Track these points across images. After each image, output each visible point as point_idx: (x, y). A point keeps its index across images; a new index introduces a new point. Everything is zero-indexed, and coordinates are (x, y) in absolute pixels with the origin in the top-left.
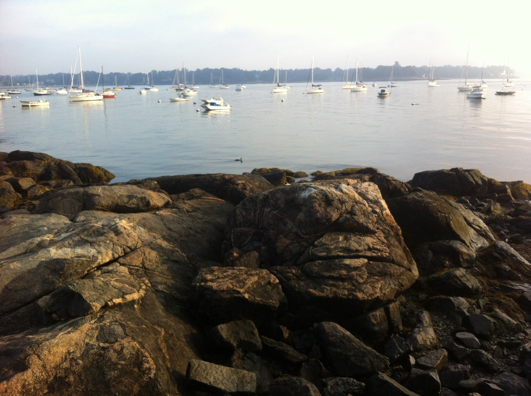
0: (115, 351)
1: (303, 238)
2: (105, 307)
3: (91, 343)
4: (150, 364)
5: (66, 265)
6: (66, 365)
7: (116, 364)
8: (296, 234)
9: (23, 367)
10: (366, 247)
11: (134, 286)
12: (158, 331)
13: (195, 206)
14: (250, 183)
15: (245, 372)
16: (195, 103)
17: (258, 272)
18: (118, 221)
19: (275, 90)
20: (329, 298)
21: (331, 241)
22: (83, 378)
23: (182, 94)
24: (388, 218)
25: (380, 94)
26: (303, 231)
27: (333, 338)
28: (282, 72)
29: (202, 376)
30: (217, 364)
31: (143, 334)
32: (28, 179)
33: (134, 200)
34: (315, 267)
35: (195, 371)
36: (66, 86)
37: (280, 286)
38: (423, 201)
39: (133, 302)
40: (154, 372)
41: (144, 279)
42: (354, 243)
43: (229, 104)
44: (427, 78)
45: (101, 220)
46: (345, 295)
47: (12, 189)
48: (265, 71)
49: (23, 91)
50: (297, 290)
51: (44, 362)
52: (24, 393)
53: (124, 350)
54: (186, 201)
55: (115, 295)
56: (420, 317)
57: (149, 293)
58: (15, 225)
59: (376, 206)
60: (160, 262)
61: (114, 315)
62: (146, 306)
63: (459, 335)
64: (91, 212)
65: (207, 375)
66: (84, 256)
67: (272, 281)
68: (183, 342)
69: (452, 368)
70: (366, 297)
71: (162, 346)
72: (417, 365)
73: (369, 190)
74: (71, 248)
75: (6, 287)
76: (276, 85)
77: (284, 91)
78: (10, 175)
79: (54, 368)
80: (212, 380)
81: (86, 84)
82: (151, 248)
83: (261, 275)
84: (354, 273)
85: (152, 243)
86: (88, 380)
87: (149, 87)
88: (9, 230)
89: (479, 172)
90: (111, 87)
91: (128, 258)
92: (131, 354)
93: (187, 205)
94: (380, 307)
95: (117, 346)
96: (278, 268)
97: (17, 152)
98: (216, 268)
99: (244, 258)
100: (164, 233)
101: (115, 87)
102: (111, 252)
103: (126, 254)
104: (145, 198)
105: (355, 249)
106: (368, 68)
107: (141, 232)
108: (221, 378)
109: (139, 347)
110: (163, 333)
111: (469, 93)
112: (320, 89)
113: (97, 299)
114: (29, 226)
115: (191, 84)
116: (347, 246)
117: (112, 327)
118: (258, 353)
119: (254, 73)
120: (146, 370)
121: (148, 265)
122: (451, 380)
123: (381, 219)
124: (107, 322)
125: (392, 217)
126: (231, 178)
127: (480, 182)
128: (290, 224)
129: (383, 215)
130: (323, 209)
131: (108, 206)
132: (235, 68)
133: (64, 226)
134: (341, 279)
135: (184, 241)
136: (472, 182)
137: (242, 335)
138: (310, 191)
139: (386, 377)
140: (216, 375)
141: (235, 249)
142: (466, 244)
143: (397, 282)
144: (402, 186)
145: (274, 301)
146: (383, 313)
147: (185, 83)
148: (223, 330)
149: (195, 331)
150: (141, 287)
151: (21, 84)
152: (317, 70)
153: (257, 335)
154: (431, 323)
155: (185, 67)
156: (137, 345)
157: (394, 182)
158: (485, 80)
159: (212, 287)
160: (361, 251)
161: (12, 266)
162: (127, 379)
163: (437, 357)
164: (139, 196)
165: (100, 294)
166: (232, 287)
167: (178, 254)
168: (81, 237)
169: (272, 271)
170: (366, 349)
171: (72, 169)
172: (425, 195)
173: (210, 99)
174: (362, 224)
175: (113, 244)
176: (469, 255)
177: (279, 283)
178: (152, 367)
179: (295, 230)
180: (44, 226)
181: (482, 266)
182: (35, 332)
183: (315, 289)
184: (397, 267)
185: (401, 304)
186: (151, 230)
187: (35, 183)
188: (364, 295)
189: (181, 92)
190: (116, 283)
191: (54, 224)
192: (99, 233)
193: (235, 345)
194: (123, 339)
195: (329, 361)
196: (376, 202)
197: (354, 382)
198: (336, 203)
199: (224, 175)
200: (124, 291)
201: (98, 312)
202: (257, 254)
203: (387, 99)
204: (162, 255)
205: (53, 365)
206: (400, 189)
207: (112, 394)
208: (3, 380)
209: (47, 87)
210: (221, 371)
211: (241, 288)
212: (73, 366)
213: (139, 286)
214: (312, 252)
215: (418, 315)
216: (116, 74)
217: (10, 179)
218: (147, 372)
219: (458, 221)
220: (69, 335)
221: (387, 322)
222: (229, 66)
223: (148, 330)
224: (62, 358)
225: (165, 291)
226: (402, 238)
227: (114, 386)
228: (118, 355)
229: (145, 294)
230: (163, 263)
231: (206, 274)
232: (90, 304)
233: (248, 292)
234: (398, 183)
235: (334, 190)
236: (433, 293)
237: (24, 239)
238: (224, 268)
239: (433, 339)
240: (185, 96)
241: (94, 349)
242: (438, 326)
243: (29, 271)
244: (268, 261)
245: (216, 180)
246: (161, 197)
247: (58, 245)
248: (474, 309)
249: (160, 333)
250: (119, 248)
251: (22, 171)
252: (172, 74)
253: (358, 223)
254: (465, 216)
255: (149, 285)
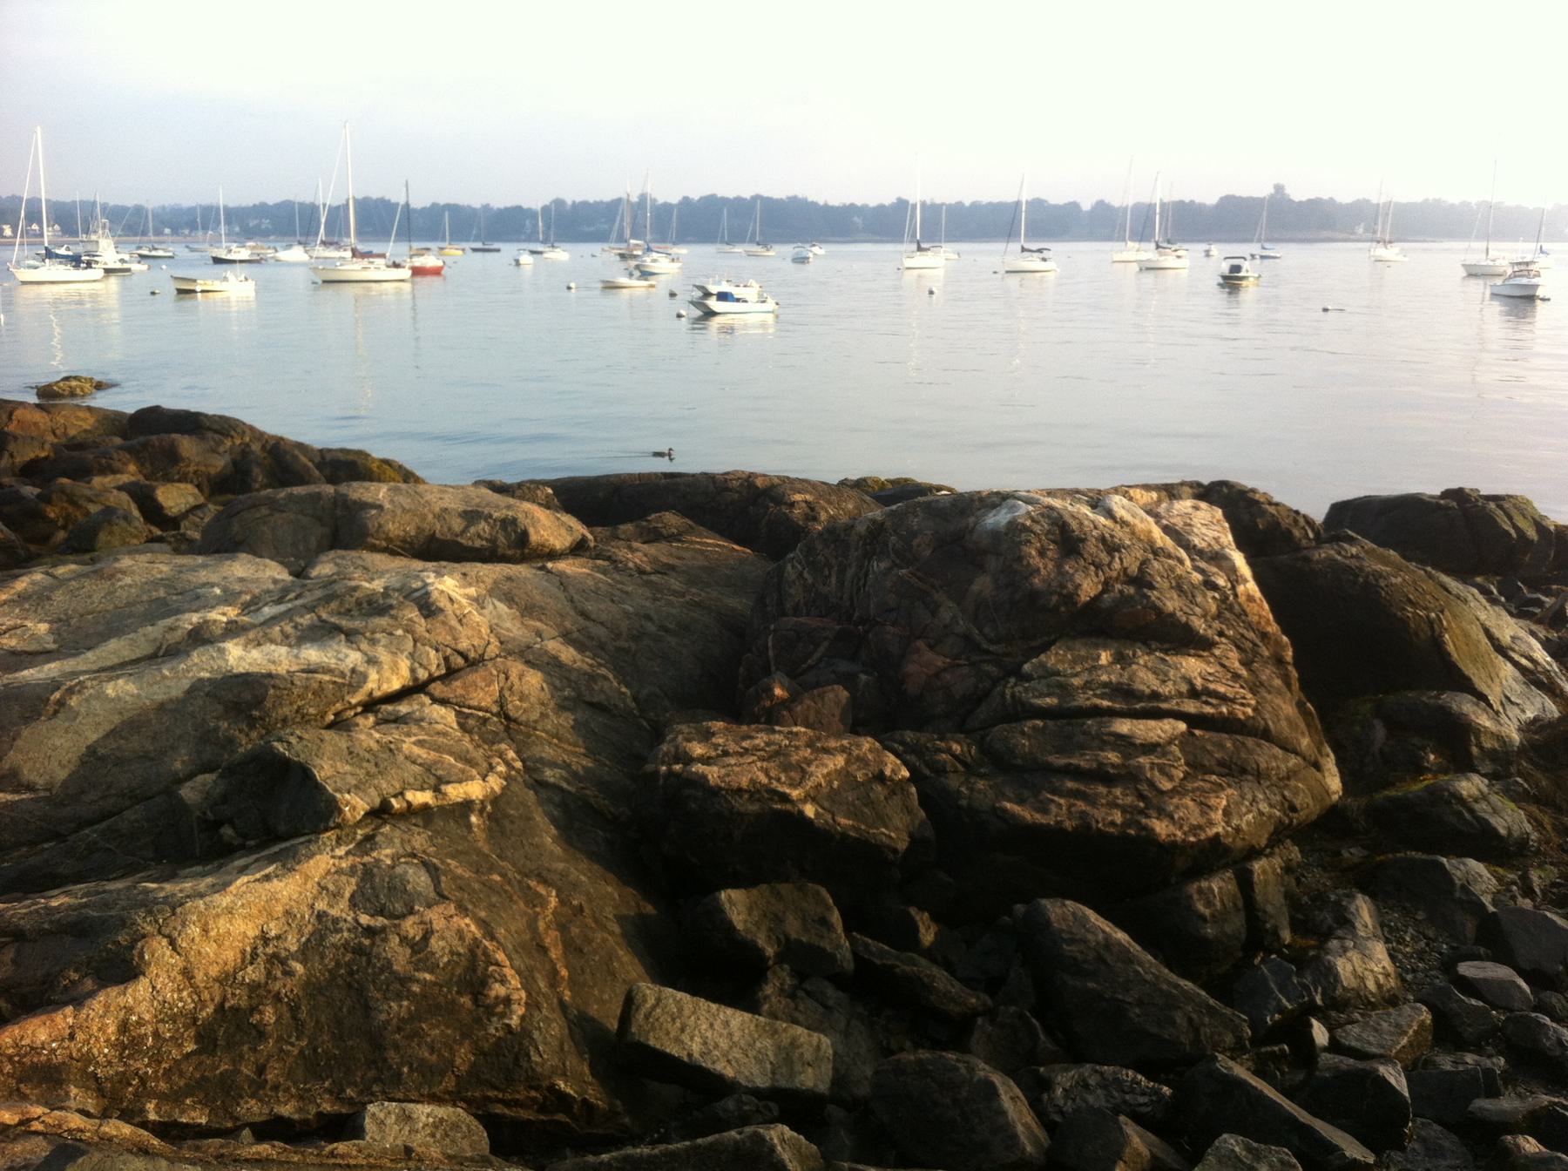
0: (404, 940)
1: (987, 652)
2: (381, 813)
3: (333, 912)
4: (509, 985)
5: (272, 691)
6: (253, 974)
7: (405, 980)
8: (967, 638)
9: (124, 969)
10: (1184, 688)
11: (470, 762)
12: (539, 895)
13: (664, 559)
14: (830, 503)
15: (800, 1030)
16: (672, 295)
17: (845, 742)
18: (431, 578)
19: (908, 263)
20: (1063, 831)
21: (1074, 662)
22: (303, 1015)
23: (637, 267)
24: (1252, 609)
25: (1225, 278)
26: (987, 630)
27: (1073, 948)
28: (932, 210)
29: (668, 1033)
30: (714, 1001)
31: (494, 899)
32: (182, 486)
33: (483, 527)
34: (1024, 739)
35: (647, 1017)
36: (303, 239)
37: (913, 790)
38: (1361, 569)
39: (467, 805)
40: (520, 1010)
41: (503, 746)
42: (1145, 673)
43: (773, 297)
44: (1370, 235)
45: (381, 574)
46: (1113, 823)
47: (136, 513)
48: (881, 207)
49: (181, 251)
50: (964, 802)
51: (187, 960)
52: (125, 1048)
53: (433, 941)
54: (636, 545)
55: (412, 780)
56: (1346, 909)
57: (515, 788)
58: (128, 580)
59: (1215, 570)
60: (552, 704)
61: (406, 837)
62: (506, 823)
63: (1466, 969)
64: (353, 554)
65: (683, 1030)
66: (327, 670)
67: (888, 772)
68: (612, 933)
69: (1446, 1063)
70: (1179, 833)
71: (548, 940)
72: (1335, 1046)
73: (1195, 521)
74: (290, 646)
75: (92, 750)
76: (914, 247)
77: (938, 262)
78: (131, 473)
79: (216, 980)
80: (696, 1047)
81: (361, 234)
82: (528, 663)
83: (856, 752)
84: (1143, 760)
85: (529, 647)
86: (317, 1022)
87: (540, 248)
88: (110, 593)
89: (1528, 502)
90: (433, 246)
91: (458, 683)
92: (452, 953)
93: (638, 555)
94: (1225, 867)
95: (410, 927)
96: (909, 736)
97: (155, 410)
98: (718, 725)
99: (806, 705)
100: (568, 624)
101: (445, 245)
102: (408, 663)
103: (451, 673)
104: (514, 521)
105: (1147, 691)
106: (1192, 202)
107: (499, 617)
108: (724, 1044)
109: (479, 935)
110: (553, 902)
111: (1499, 281)
112: (1044, 260)
113: (356, 787)
114: (167, 583)
115: (664, 241)
116: (1125, 680)
117: (399, 870)
118: (839, 980)
119: (851, 210)
120: (497, 1005)
121: (517, 708)
122: (1446, 1100)
123: (1229, 609)
124: (385, 854)
125: (1266, 606)
126: (773, 487)
127: (1532, 533)
128: (948, 611)
129: (1236, 596)
130: (1050, 566)
131: (404, 541)
132: (795, 197)
133: (271, 587)
134: (1103, 776)
135: (627, 651)
136: (1507, 533)
137: (793, 927)
138: (1013, 508)
139: (1241, 1072)
140: (709, 1034)
141: (778, 675)
142: (1491, 706)
143: (1278, 798)
144: (1296, 522)
145: (896, 830)
146: (1232, 887)
147: (648, 237)
148: (737, 905)
149: (649, 909)
150: (491, 768)
151: (175, 232)
152: (1037, 205)
153: (840, 930)
154: (1379, 932)
155: (649, 190)
156: (473, 928)
157: (1272, 509)
158: (1546, 246)
159: (704, 777)
160: (1167, 699)
161: (110, 690)
162: (437, 1027)
163: (1398, 1026)
164: (496, 515)
165: (368, 774)
166: (765, 780)
167: (606, 685)
168: (319, 617)
169: (890, 743)
170: (1177, 986)
171: (310, 464)
172: (1367, 552)
173: (719, 283)
174: (1172, 615)
175: (415, 641)
176: (1498, 737)
177: (909, 780)
178: (515, 997)
179: (962, 626)
180: (213, 585)
181: (1539, 775)
182: (171, 877)
183: (1021, 801)
184: (1277, 751)
185: (1288, 869)
186: (528, 610)
187: (202, 500)
188: (1172, 829)
189: (633, 263)
190: (416, 750)
191: (241, 580)
192: (376, 607)
193: (770, 951)
194: (429, 906)
195: (1061, 1015)
196: (1218, 558)
197: (1139, 1083)
198: (1092, 547)
199: (751, 475)
200: (440, 772)
201: (359, 824)
202: (844, 694)
203: (1249, 291)
204: (557, 683)
205: (214, 971)
206: (1290, 532)
207: (390, 1067)
208: (66, 1004)
209: (250, 239)
210: (727, 1024)
211: (793, 785)
212: (276, 979)
213: (485, 765)
214: (1013, 695)
215: (1338, 903)
216: (448, 207)
217: (132, 483)
218: (500, 1008)
219: (1467, 635)
220: (267, 885)
221: (1242, 914)
222: (777, 188)
223: (508, 888)
224: (243, 952)
225: (565, 785)
226: (1295, 674)
227: (397, 1047)
228: (414, 953)
229: (503, 788)
230: (562, 707)
231: (689, 740)
232: (334, 798)
233: (814, 800)
234: (1284, 514)
235: (1086, 510)
236: (1388, 842)
237: (150, 618)
238: (745, 728)
239: (1387, 975)
240: (645, 275)
241: (341, 930)
242: (1401, 941)
243: (161, 707)
244: (877, 716)
245: (727, 489)
246: (563, 524)
247: (251, 635)
248: (1513, 898)
249: (544, 903)
250: (432, 653)
251: (167, 465)
252: (610, 210)
253: (1159, 612)
254: (1487, 623)
255: (519, 765)
